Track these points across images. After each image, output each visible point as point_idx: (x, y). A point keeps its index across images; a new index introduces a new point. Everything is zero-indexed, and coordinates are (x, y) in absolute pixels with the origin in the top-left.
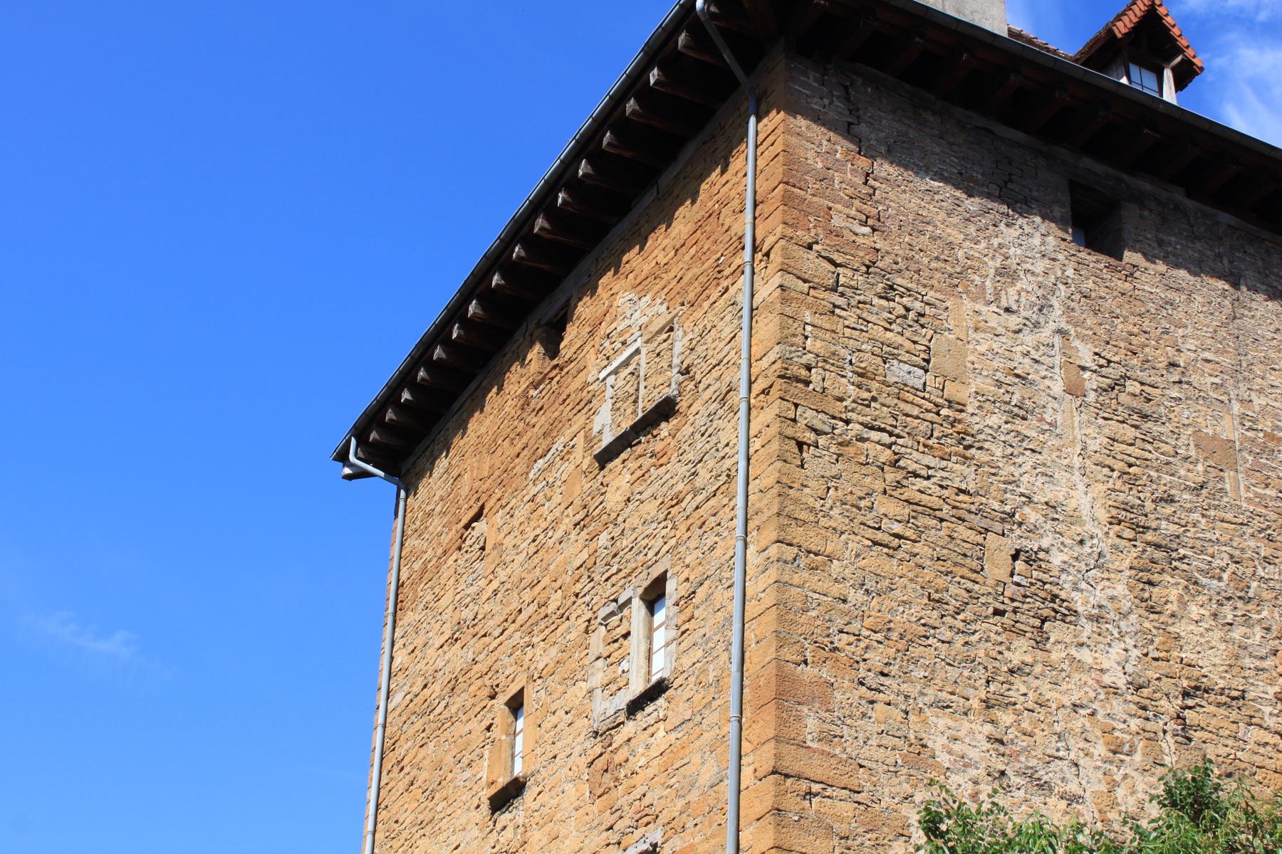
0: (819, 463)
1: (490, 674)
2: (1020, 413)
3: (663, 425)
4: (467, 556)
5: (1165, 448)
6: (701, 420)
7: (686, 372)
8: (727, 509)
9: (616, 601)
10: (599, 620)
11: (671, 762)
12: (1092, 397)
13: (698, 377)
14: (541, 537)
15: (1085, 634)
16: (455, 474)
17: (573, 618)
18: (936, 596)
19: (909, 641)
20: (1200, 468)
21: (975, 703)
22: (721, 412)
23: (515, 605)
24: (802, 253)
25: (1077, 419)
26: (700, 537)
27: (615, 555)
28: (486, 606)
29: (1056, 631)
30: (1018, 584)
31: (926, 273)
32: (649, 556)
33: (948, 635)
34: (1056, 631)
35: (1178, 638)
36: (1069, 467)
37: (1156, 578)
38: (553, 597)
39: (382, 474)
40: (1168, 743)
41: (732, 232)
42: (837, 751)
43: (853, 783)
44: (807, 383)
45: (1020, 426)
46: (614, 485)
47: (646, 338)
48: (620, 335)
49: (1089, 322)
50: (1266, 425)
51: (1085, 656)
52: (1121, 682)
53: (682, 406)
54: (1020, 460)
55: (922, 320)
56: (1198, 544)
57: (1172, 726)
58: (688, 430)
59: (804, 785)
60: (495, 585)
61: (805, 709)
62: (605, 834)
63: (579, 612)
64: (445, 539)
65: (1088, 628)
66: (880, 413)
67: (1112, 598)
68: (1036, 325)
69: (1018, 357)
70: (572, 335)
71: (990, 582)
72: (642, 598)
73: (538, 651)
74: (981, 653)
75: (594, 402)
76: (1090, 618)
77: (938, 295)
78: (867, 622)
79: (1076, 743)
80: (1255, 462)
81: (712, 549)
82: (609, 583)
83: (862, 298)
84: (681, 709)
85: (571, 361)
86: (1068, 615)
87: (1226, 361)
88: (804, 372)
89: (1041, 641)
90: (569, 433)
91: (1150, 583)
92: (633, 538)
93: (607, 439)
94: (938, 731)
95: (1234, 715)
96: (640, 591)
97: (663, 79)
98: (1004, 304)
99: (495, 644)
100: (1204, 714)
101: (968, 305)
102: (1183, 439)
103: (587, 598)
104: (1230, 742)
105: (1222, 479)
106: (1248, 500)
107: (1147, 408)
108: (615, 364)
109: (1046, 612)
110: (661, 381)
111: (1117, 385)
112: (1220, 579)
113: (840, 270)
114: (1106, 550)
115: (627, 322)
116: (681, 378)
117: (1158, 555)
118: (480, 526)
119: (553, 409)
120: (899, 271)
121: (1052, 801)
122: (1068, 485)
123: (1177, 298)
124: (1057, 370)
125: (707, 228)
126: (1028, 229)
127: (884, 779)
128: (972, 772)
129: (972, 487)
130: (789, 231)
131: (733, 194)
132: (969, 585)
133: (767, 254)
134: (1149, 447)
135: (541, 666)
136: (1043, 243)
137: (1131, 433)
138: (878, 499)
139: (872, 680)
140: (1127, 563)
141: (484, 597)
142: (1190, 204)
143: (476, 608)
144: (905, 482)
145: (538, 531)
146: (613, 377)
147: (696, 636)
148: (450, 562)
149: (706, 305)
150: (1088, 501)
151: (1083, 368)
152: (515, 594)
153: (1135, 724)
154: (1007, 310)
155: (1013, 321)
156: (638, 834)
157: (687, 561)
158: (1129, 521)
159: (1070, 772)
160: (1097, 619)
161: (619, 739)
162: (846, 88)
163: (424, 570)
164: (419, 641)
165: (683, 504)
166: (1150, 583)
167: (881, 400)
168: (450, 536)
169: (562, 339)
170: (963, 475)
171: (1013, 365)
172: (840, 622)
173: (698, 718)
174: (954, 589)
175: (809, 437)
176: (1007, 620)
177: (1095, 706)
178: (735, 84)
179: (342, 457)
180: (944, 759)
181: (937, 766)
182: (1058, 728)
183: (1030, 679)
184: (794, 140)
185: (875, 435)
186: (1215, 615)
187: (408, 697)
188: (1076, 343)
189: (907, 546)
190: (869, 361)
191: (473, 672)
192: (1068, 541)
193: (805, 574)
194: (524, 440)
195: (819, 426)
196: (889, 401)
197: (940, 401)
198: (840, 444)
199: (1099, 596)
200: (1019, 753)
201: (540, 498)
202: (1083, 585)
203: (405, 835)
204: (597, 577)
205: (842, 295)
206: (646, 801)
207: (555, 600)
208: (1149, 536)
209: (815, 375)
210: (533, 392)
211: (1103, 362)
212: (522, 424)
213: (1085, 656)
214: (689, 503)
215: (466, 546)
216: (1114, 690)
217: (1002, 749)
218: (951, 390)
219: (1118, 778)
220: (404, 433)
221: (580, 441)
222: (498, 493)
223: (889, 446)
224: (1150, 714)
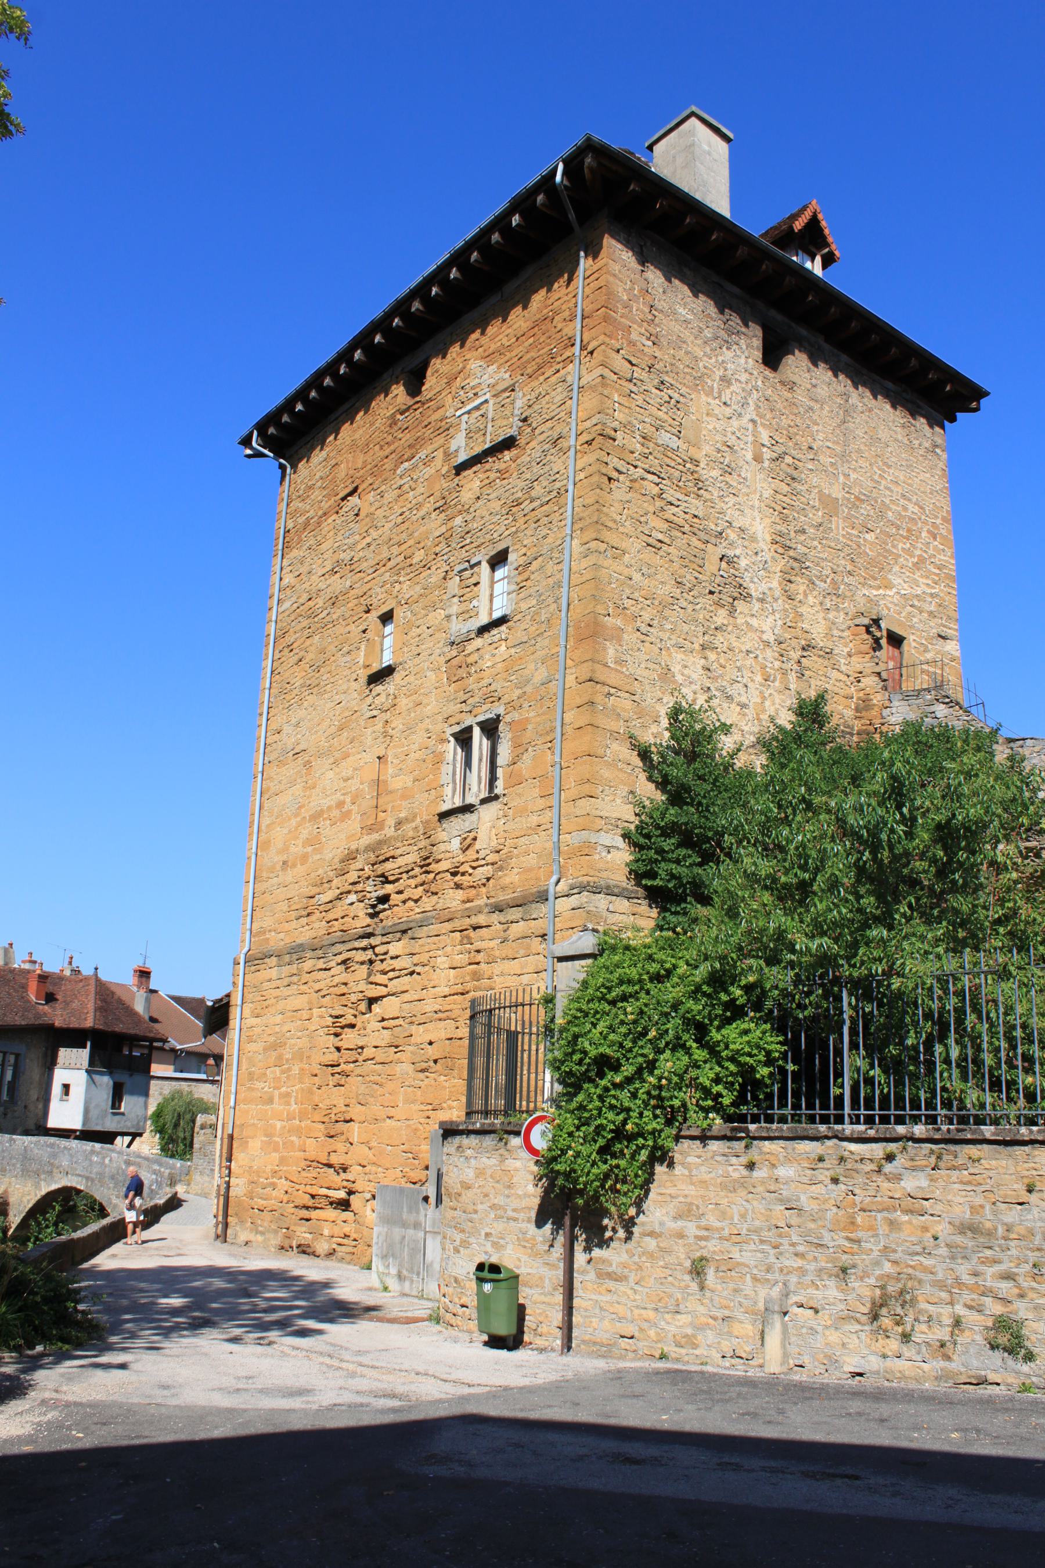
0: (619, 492)
1: (365, 597)
2: (728, 470)
3: (506, 452)
4: (343, 519)
5: (803, 499)
6: (537, 454)
7: (525, 420)
8: (557, 514)
9: (468, 561)
10: (455, 572)
11: (510, 666)
12: (766, 464)
13: (534, 425)
14: (407, 513)
15: (756, 609)
16: (333, 462)
17: (434, 568)
18: (679, 580)
19: (664, 606)
20: (820, 513)
21: (697, 646)
22: (553, 451)
23: (385, 554)
24: (614, 355)
25: (758, 477)
26: (536, 529)
27: (468, 532)
28: (361, 553)
29: (740, 605)
30: (722, 576)
31: (681, 375)
32: (495, 535)
33: (684, 604)
34: (740, 605)
35: (801, 615)
36: (752, 507)
37: (793, 578)
38: (417, 553)
39: (271, 455)
40: (792, 677)
41: (564, 333)
42: (624, 669)
43: (631, 689)
44: (614, 440)
45: (728, 478)
46: (467, 486)
47: (494, 393)
48: (472, 388)
49: (768, 416)
50: (856, 491)
51: (754, 622)
52: (772, 639)
53: (522, 441)
54: (726, 500)
55: (679, 406)
56: (816, 560)
57: (795, 667)
58: (525, 459)
59: (606, 689)
60: (368, 540)
61: (608, 643)
62: (459, 706)
63: (439, 565)
64: (325, 505)
65: (757, 606)
66: (653, 463)
67: (770, 589)
68: (740, 415)
69: (729, 434)
70: (431, 383)
71: (708, 574)
72: (488, 562)
73: (405, 587)
74: (701, 616)
75: (451, 430)
76: (758, 600)
77: (688, 390)
78: (643, 593)
79: (747, 674)
80: (849, 513)
81: (545, 537)
82: (463, 550)
83: (646, 388)
84: (519, 634)
85: (431, 400)
86: (747, 597)
87: (838, 449)
88: (613, 433)
89: (732, 612)
90: (430, 448)
91: (790, 581)
92: (482, 522)
93: (462, 457)
94: (676, 660)
95: (826, 663)
96: (487, 557)
97: (523, 223)
98: (723, 400)
99: (369, 578)
100: (811, 661)
101: (704, 398)
102: (813, 496)
103: (445, 557)
104: (823, 678)
105: (831, 521)
106: (843, 535)
107: (795, 474)
108: (468, 408)
109: (736, 595)
110: (505, 423)
111: (779, 458)
112: (825, 582)
113: (635, 368)
114: (769, 560)
115: (477, 381)
116: (521, 424)
117: (796, 565)
118: (354, 500)
119: (416, 430)
120: (667, 372)
121: (733, 706)
122: (750, 516)
123: (816, 406)
124: (749, 445)
125: (543, 327)
126: (738, 353)
127: (647, 688)
128: (693, 687)
129: (701, 515)
130: (607, 340)
131: (564, 307)
132: (697, 575)
133: (592, 353)
134: (794, 498)
135: (407, 596)
136: (746, 363)
137: (786, 489)
138: (650, 516)
139: (644, 628)
140: (779, 569)
141: (360, 547)
142: (827, 347)
143: (353, 553)
144: (665, 508)
145: (404, 509)
146: (466, 416)
147: (532, 591)
148: (330, 521)
149: (542, 379)
150: (761, 528)
151: (763, 445)
152: (385, 548)
153: (777, 664)
154: (725, 403)
155: (728, 411)
156: (485, 707)
157: (525, 543)
158: (781, 543)
159: (743, 690)
160: (762, 600)
161: (471, 647)
162: (641, 246)
163: (307, 524)
164: (304, 569)
165: (522, 506)
166: (790, 581)
167: (654, 454)
168: (330, 503)
169: (423, 384)
170: (696, 506)
171: (725, 439)
172: (628, 592)
173: (533, 642)
174: (688, 577)
175: (615, 475)
176: (715, 597)
177: (758, 652)
178: (570, 230)
179: (246, 442)
180: (679, 678)
181: (675, 682)
182: (738, 664)
183: (725, 634)
184: (611, 279)
185: (650, 477)
186: (821, 604)
187: (296, 605)
188: (760, 429)
189: (665, 548)
190: (649, 430)
191: (350, 595)
192: (750, 553)
193: (610, 561)
194: (392, 447)
195: (621, 469)
196: (659, 456)
197: (686, 458)
198: (631, 481)
199: (763, 587)
200: (717, 677)
201: (406, 487)
202: (756, 580)
203: (296, 692)
204: (454, 545)
205: (635, 385)
206: (492, 688)
207: (419, 556)
208: (791, 553)
209: (619, 435)
210: (399, 417)
211: (774, 442)
212: (390, 437)
213: (754, 622)
214: (527, 506)
215: (342, 512)
216: (767, 644)
217: (709, 674)
218: (693, 452)
219: (766, 695)
220: (294, 430)
221: (439, 455)
222: (370, 480)
223: (657, 485)
224: (785, 659)
